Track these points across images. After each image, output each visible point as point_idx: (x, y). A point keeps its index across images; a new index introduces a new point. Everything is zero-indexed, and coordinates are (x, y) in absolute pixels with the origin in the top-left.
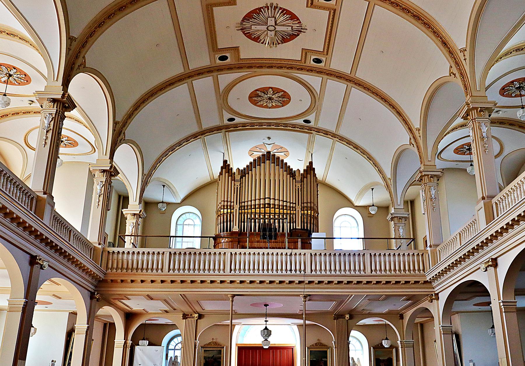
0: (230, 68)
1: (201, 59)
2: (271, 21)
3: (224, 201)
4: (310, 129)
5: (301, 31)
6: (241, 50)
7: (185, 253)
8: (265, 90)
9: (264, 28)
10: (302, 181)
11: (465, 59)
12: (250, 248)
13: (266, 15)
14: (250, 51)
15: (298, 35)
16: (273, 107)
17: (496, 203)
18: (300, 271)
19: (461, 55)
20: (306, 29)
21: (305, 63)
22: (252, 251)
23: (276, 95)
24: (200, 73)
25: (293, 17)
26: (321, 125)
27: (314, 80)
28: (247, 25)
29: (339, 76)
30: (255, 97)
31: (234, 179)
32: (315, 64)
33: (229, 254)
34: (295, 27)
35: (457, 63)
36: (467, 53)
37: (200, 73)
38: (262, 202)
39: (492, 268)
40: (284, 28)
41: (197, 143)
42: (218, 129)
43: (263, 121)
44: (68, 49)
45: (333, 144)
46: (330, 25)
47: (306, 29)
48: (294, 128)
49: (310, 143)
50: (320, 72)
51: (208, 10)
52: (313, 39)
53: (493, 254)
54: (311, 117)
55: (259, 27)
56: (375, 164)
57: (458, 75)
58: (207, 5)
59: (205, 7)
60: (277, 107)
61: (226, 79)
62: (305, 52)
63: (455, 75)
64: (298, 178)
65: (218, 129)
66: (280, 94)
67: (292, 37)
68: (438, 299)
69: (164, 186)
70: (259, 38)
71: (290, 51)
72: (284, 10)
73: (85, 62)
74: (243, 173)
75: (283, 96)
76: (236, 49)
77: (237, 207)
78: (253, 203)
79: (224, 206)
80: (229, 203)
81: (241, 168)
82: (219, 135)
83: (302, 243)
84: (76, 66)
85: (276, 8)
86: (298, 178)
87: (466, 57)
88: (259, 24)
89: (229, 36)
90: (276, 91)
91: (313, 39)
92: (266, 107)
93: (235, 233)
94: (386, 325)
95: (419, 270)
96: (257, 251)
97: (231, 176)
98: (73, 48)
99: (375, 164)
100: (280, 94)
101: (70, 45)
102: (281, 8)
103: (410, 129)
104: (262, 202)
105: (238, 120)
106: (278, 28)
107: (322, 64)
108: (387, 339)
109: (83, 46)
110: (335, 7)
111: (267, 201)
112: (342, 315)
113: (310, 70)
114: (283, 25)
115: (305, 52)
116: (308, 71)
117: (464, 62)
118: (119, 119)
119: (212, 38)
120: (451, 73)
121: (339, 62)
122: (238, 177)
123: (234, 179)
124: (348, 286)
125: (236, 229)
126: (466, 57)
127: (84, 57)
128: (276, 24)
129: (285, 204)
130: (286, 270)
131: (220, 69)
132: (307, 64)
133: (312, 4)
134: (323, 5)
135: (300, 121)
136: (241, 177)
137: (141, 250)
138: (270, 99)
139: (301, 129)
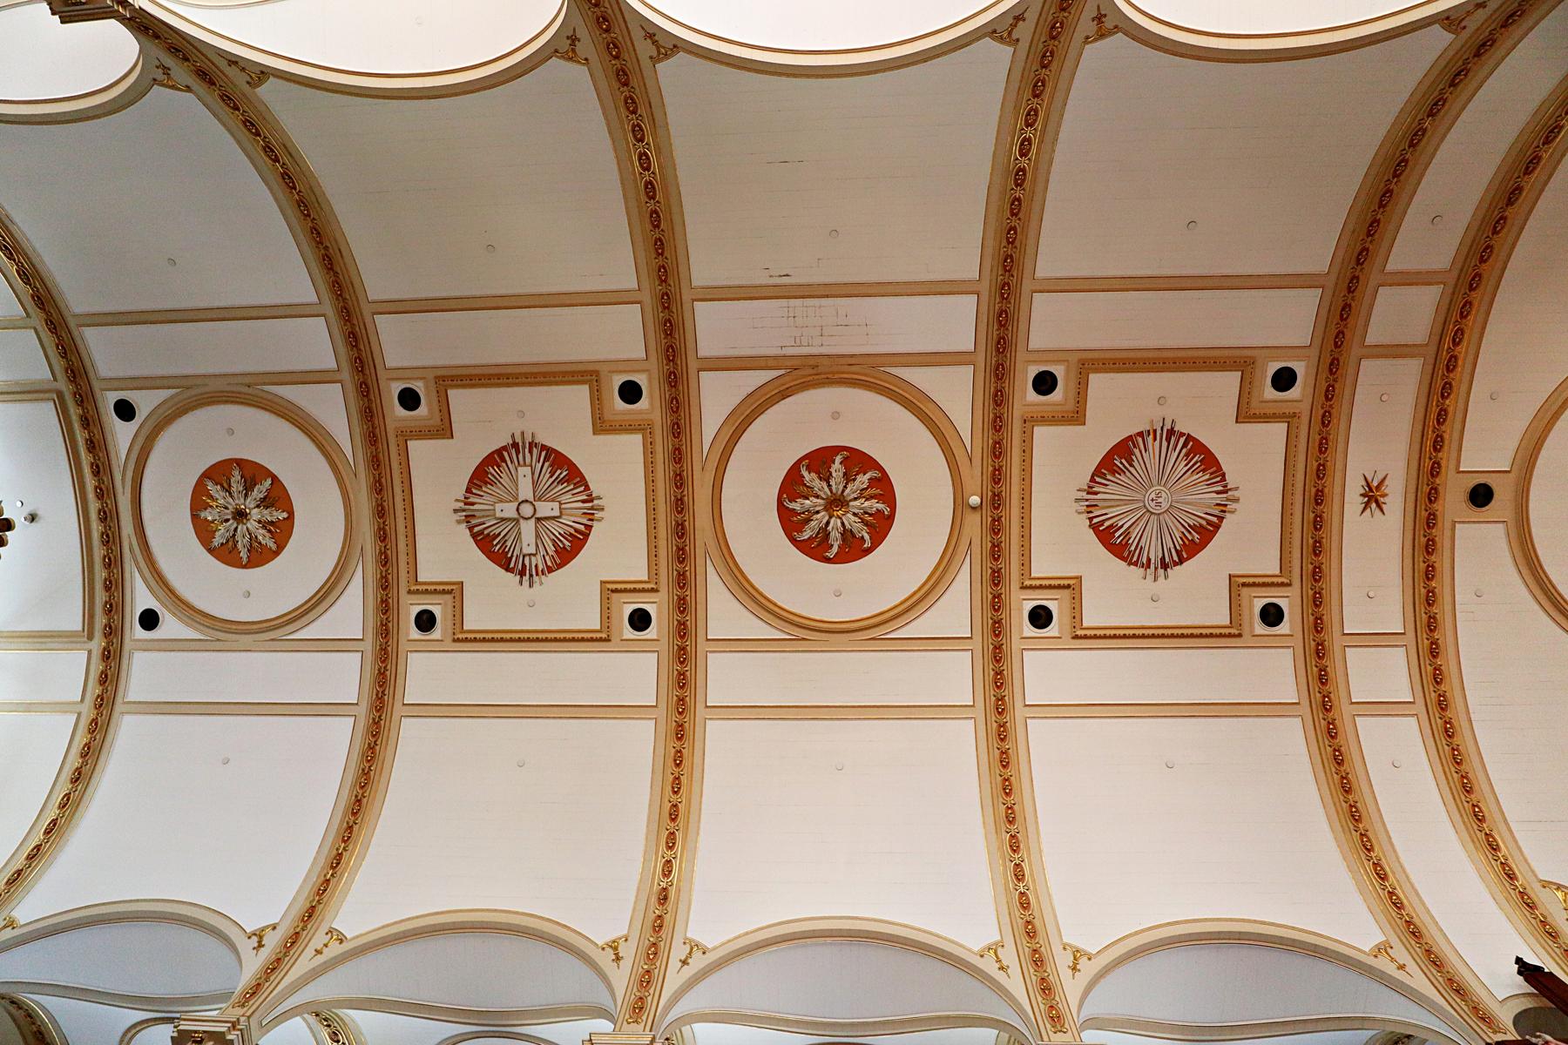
1: (402, 346)
4: (113, 632)
5: (522, 574)
11: (318, 952)
19: (319, 939)
20: (531, 586)
21: (409, 592)
32: (404, 614)
35: (295, 938)
36: (335, 949)
44: (234, 61)
45: (60, 707)
46: (562, 636)
47: (531, 586)
50: (997, 628)
51: (583, 373)
57: (265, 953)
58: (597, 373)
59: (597, 367)
62: (453, 591)
63: (260, 945)
72: (586, 536)
73: (173, 87)
84: (169, 61)
87: (325, 950)
88: (535, 484)
89: (484, 421)
98: (232, 72)
101: (243, 69)
102: (589, 527)
105: (122, 435)
106: (528, 529)
109: (226, 98)
110: (615, 639)
113: (997, 604)
117: (310, 951)
118: (268, 92)
120: (259, 935)
121: (1045, 671)
126: (325, 950)
127: (188, 89)
128: (538, 519)
132: (405, 599)
134: (614, 616)
135: (142, 598)
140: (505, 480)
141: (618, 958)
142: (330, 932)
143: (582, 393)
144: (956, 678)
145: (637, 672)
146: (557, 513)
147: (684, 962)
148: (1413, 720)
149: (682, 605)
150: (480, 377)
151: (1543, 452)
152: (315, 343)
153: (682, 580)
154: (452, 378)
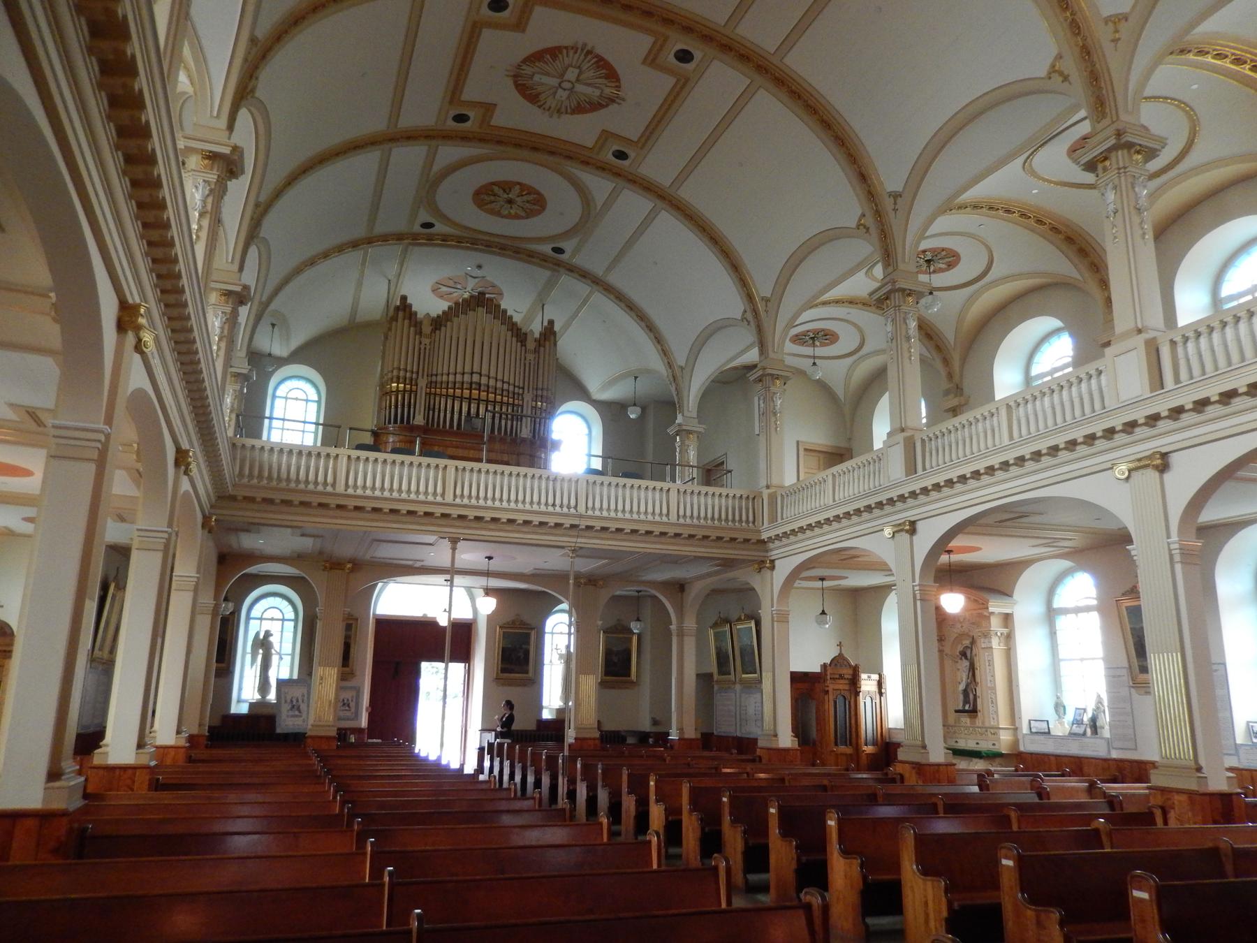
0: (465, 138)
2: (571, 74)
3: (399, 369)
6: (498, 111)
7: (319, 454)
8: (506, 186)
9: (554, 82)
10: (536, 351)
12: (489, 461)
13: (567, 61)
14: (514, 113)
15: (607, 106)
16: (509, 216)
17: (923, 441)
18: (569, 507)
22: (492, 467)
23: (525, 198)
24: (410, 137)
25: (612, 75)
26: (579, 261)
27: (601, 187)
28: (527, 70)
29: (648, 188)
30: (485, 196)
31: (420, 333)
32: (618, 162)
33: (345, 459)
34: (607, 91)
37: (410, 137)
38: (467, 378)
39: (907, 536)
40: (589, 90)
41: (355, 256)
42: (399, 237)
43: (480, 237)
48: (531, 257)
49: (550, 285)
50: (618, 174)
52: (626, 121)
53: (910, 515)
54: (568, 245)
55: (545, 79)
56: (658, 339)
57: (873, 230)
60: (517, 217)
61: (449, 153)
62: (606, 135)
63: (868, 229)
64: (531, 345)
65: (399, 237)
66: (531, 197)
67: (594, 106)
68: (773, 568)
69: (273, 325)
70: (537, 95)
71: (580, 130)
74: (438, 323)
75: (535, 202)
76: (489, 108)
77: (422, 383)
78: (459, 378)
79: (398, 378)
80: (408, 375)
81: (434, 314)
82: (398, 249)
83: (423, 444)
85: (589, 52)
86: (531, 345)
88: (547, 74)
90: (526, 190)
91: (626, 121)
92: (499, 214)
93: (418, 427)
94: (303, 578)
95: (747, 522)
96: (500, 468)
97: (415, 326)
99: (658, 339)
100: (531, 197)
103: (750, 297)
104: (451, 378)
105: (440, 228)
106: (580, 88)
107: (626, 163)
108: (638, 620)
111: (476, 378)
112: (339, 564)
113: (602, 168)
114: (589, 85)
115: (606, 135)
116: (598, 168)
118: (260, 34)
119: (458, 80)
121: (658, 165)
122: (427, 329)
123: (420, 333)
124: (554, 531)
125: (419, 420)
128: (578, 80)
129: (506, 386)
130: (509, 501)
131: (447, 137)
133: (654, 60)
135: (546, 249)
136: (434, 331)
137: (704, 489)
138: (510, 202)
139: (543, 260)
140: (540, 89)
141: (1066, 78)
142: (1107, 20)
143: (487, 34)
144: (634, 204)
145: (720, 80)
146: (577, 71)
147: (1115, 41)
148: (762, 91)
149: (688, 29)
150: (465, 57)
151: (470, 226)
152: (409, 158)
153: (668, 21)
154: (454, 93)
